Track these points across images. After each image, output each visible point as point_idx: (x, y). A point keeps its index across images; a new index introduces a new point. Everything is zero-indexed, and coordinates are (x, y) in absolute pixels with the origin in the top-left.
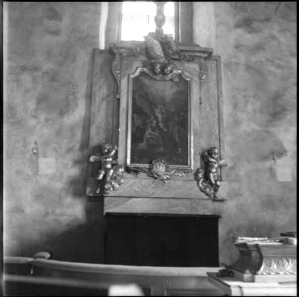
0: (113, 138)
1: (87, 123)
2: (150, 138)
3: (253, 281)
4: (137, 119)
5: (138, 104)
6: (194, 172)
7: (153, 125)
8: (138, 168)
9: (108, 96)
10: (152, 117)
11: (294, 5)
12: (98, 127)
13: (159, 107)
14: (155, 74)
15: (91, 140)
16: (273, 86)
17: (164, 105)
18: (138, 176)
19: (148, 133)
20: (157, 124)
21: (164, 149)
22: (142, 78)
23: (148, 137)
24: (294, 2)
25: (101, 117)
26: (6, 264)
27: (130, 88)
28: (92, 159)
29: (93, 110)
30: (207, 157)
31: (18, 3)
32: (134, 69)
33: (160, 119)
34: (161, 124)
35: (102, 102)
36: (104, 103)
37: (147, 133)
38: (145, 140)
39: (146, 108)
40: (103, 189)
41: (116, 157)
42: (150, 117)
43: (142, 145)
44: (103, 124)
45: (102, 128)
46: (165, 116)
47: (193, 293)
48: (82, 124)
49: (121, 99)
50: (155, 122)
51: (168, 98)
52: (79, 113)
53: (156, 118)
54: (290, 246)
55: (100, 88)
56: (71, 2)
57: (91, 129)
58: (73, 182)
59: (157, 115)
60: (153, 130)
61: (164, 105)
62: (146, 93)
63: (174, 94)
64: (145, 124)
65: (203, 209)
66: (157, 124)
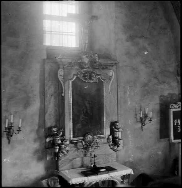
0: (61, 127)
1: (43, 112)
3: (145, 125)
6: (107, 138)
8: (77, 140)
9: (55, 92)
12: (50, 115)
14: (86, 79)
15: (46, 123)
18: (83, 182)
20: (87, 111)
25: (51, 108)
28: (48, 140)
29: (46, 104)
30: (113, 126)
32: (72, 76)
34: (89, 111)
35: (51, 97)
36: (53, 98)
38: (80, 122)
40: (58, 157)
41: (64, 135)
43: (79, 126)
44: (53, 112)
45: (52, 115)
48: (38, 112)
49: (65, 96)
52: (36, 106)
53: (86, 107)
55: (49, 87)
57: (46, 117)
58: (36, 151)
65: (112, 158)
66: (87, 111)
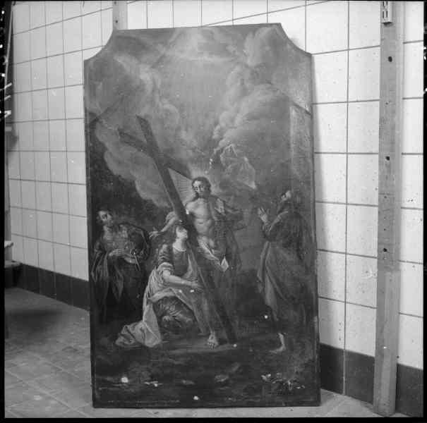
10: (172, 217)
13: (195, 173)
16: (101, 266)
19: (161, 281)
21: (221, 342)
23: (158, 296)
26: (97, 403)
31: (43, 2)
33: (201, 224)
42: (164, 213)
43: (182, 305)
46: (221, 209)
47: (402, 33)
50: (181, 235)
51: (230, 134)
53: (188, 222)
59: (190, 208)
60: (180, 271)
62: (143, 122)
64: (145, 246)
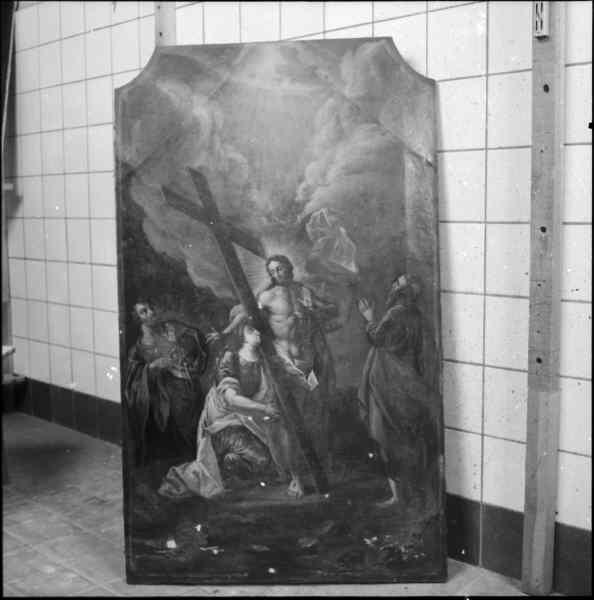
2: (228, 430)
4: (158, 328)
5: (157, 242)
7: (246, 355)
10: (239, 313)
11: (588, 592)
13: (271, 250)
17: (300, 236)
21: (307, 490)
22: (169, 89)
23: (219, 425)
24: (590, 590)
27: (9, 71)
33: (280, 323)
37: (212, 404)
39: (201, 267)
46: (307, 301)
50: (251, 338)
53: (260, 320)
54: (243, 53)
56: (591, 505)
61: (300, 236)
63: (351, 171)
64: (201, 355)
